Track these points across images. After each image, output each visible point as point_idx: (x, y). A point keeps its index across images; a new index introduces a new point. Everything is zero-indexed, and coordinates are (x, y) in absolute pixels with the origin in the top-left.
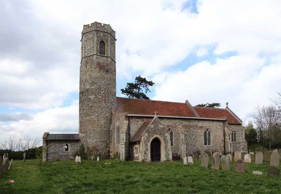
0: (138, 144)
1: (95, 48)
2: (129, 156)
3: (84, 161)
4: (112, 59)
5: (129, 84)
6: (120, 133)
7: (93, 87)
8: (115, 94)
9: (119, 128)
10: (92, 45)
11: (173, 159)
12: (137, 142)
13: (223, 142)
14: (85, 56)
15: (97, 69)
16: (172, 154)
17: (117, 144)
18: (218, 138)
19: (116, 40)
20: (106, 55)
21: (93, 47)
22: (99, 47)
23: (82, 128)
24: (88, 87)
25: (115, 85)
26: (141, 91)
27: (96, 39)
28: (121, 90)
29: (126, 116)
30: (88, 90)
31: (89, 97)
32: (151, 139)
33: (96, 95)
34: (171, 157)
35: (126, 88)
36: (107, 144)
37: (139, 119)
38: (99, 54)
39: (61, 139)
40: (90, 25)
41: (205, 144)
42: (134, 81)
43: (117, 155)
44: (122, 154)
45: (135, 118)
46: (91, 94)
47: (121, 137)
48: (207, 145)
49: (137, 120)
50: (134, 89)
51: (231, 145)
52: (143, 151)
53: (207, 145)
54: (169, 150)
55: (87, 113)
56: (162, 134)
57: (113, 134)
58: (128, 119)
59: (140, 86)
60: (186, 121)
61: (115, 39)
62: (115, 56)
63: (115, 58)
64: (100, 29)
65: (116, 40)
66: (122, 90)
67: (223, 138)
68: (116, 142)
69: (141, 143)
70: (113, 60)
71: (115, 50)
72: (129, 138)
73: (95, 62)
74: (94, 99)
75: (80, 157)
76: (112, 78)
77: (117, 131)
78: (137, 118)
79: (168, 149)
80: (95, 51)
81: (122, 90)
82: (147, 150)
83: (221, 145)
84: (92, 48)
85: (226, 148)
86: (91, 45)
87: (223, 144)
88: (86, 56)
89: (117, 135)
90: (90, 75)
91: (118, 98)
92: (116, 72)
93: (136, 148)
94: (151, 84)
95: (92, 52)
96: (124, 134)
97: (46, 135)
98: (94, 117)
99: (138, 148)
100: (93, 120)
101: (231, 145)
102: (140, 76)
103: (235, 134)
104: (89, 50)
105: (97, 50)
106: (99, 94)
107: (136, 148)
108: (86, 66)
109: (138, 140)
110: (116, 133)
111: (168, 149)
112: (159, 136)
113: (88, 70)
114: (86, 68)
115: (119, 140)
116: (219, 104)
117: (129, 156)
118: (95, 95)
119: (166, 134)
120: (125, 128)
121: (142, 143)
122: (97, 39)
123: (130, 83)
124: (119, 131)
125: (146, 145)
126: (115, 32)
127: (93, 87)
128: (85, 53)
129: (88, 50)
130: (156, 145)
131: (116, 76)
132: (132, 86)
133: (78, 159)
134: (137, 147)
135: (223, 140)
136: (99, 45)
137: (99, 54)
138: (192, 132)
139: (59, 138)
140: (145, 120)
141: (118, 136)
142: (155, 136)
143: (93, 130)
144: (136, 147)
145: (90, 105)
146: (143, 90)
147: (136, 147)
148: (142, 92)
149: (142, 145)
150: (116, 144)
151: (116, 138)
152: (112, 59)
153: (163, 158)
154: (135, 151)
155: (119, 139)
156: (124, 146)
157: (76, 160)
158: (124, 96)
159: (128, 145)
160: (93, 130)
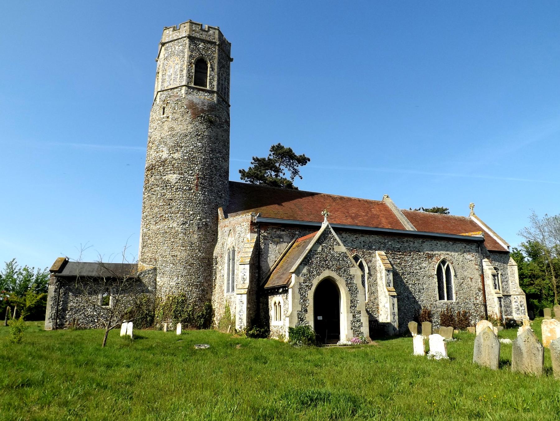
0: (281, 293)
1: (185, 72)
2: (259, 319)
3: (142, 332)
4: (222, 98)
5: (256, 160)
6: (237, 263)
7: (176, 156)
8: (227, 172)
9: (234, 251)
10: (180, 66)
11: (371, 336)
12: (279, 288)
13: (480, 294)
14: (163, 89)
15: (188, 117)
16: (368, 324)
17: (228, 291)
18: (470, 282)
19: (232, 60)
20: (208, 88)
21: (182, 71)
22: (193, 71)
23: (146, 250)
24: (165, 155)
25: (228, 154)
26: (281, 175)
27: (187, 53)
28: (240, 171)
29: (252, 222)
30: (164, 163)
31: (166, 178)
32: (315, 282)
33: (182, 174)
34: (365, 330)
35: (250, 168)
36: (203, 290)
37: (283, 231)
38: (192, 85)
39: (443, 243)
40: (220, 212)
41: (441, 297)
42: (265, 154)
43: (229, 321)
44: (240, 318)
45: (273, 229)
46: (172, 172)
47: (237, 275)
48: (444, 299)
49: (278, 233)
50: (267, 171)
51: (500, 301)
52: (296, 314)
53: (444, 299)
54: (359, 312)
55: (159, 216)
56: (343, 270)
57: (220, 268)
58: (256, 230)
59: (279, 165)
60: (394, 240)
61: (228, 56)
62: (228, 92)
63: (228, 96)
64: (198, 35)
65: (232, 60)
66: (242, 172)
67: (480, 284)
68: (225, 287)
69: (290, 291)
70: (224, 100)
71: (229, 80)
72: (259, 277)
73: (185, 102)
74: (177, 182)
75: (131, 324)
76: (220, 137)
77: (229, 260)
78: (278, 229)
79: (357, 309)
80: (185, 78)
81: (242, 172)
82: (306, 311)
83: (478, 301)
84: (178, 73)
85: (488, 308)
86: (177, 67)
87: (481, 298)
88: (166, 88)
89: (229, 269)
90: (172, 129)
91: (232, 184)
92: (229, 126)
93: (275, 303)
94: (303, 160)
95: (178, 80)
96: (248, 267)
97: (61, 263)
98: (175, 225)
99: (282, 304)
100: (173, 231)
101: (500, 301)
102: (279, 144)
103: (448, 269)
104: (173, 76)
105: (189, 77)
106: (189, 171)
107: (275, 303)
108: (164, 109)
109: (281, 283)
110: (226, 266)
111: (357, 309)
112: (334, 275)
113: (168, 117)
114: (163, 114)
115: (233, 282)
116: (446, 209)
117: (259, 319)
118: (179, 174)
119: (351, 269)
120: (246, 251)
121: (293, 293)
122: (190, 53)
123: (259, 158)
124: (234, 259)
125: (304, 299)
126: (230, 44)
127: (176, 156)
128: (162, 83)
129: (170, 76)
130: (326, 299)
131: (229, 136)
132: (263, 164)
133: (127, 328)
134: (279, 303)
135: (481, 287)
136: (194, 66)
137: (192, 85)
138: (411, 266)
139: (89, 271)
140: (297, 233)
141: (232, 272)
142: (326, 273)
143: (172, 256)
144: (277, 303)
145: (169, 196)
146: (286, 174)
147: (277, 303)
148: (284, 177)
149: (293, 298)
150: (225, 291)
151: (226, 276)
152: (222, 98)
153: (345, 333)
154: (272, 313)
155: (233, 278)
156: (245, 298)
157: (123, 332)
158: (246, 181)
159: (254, 297)
160: (172, 256)
